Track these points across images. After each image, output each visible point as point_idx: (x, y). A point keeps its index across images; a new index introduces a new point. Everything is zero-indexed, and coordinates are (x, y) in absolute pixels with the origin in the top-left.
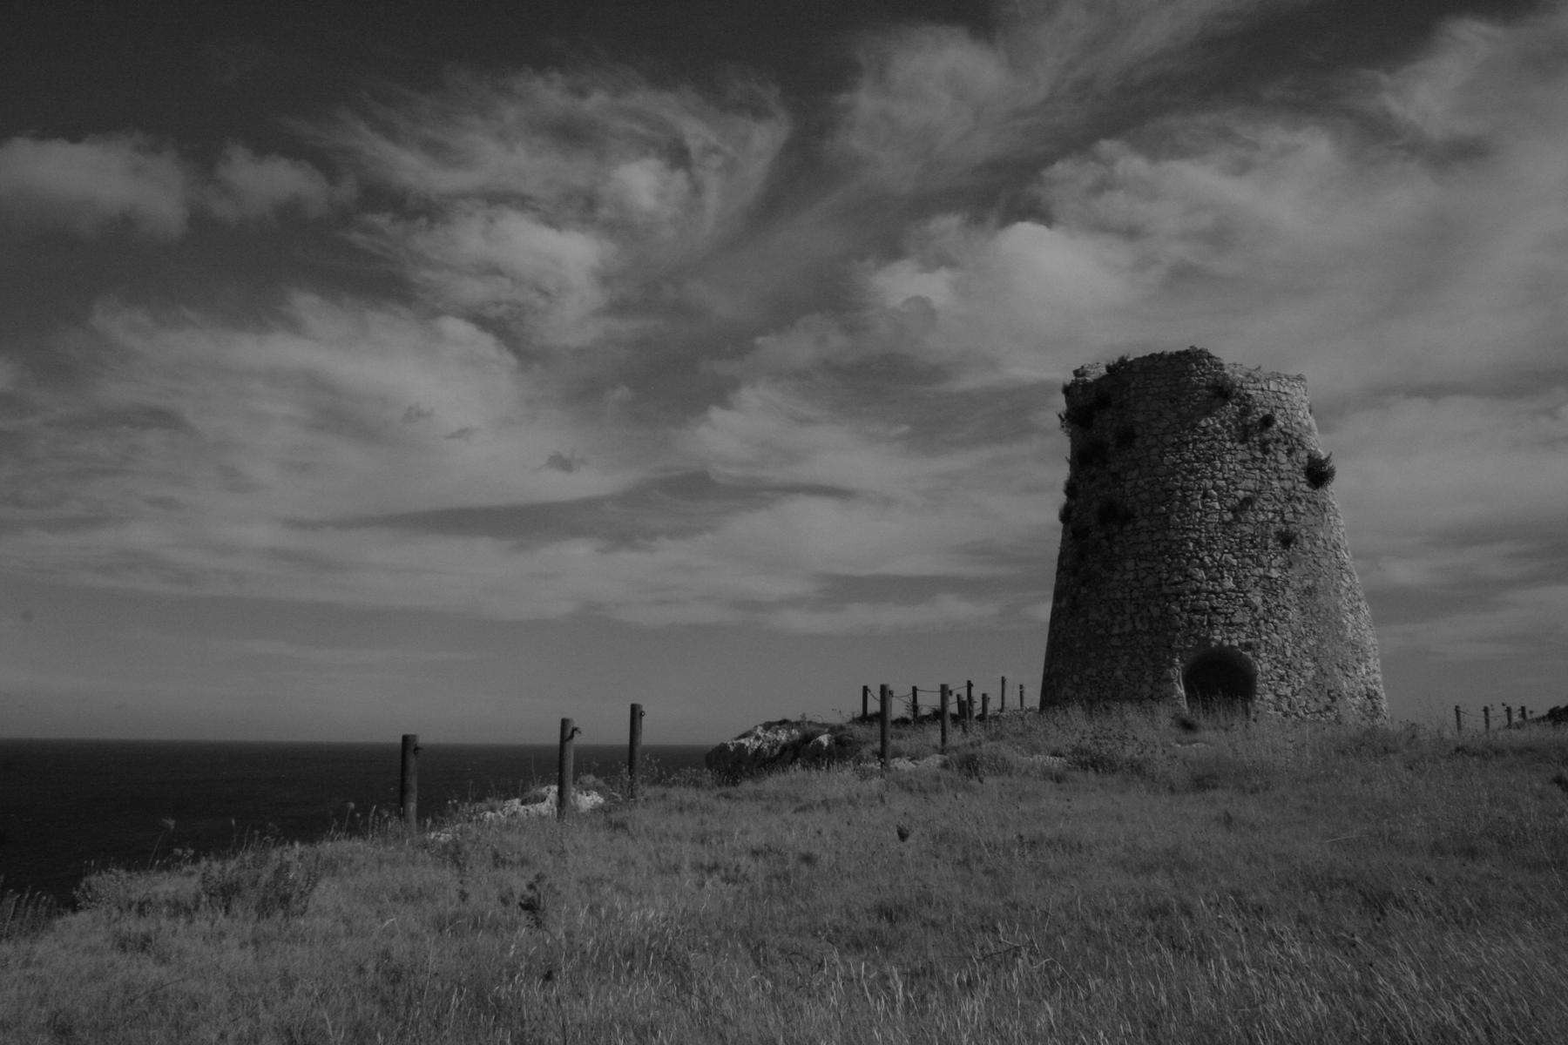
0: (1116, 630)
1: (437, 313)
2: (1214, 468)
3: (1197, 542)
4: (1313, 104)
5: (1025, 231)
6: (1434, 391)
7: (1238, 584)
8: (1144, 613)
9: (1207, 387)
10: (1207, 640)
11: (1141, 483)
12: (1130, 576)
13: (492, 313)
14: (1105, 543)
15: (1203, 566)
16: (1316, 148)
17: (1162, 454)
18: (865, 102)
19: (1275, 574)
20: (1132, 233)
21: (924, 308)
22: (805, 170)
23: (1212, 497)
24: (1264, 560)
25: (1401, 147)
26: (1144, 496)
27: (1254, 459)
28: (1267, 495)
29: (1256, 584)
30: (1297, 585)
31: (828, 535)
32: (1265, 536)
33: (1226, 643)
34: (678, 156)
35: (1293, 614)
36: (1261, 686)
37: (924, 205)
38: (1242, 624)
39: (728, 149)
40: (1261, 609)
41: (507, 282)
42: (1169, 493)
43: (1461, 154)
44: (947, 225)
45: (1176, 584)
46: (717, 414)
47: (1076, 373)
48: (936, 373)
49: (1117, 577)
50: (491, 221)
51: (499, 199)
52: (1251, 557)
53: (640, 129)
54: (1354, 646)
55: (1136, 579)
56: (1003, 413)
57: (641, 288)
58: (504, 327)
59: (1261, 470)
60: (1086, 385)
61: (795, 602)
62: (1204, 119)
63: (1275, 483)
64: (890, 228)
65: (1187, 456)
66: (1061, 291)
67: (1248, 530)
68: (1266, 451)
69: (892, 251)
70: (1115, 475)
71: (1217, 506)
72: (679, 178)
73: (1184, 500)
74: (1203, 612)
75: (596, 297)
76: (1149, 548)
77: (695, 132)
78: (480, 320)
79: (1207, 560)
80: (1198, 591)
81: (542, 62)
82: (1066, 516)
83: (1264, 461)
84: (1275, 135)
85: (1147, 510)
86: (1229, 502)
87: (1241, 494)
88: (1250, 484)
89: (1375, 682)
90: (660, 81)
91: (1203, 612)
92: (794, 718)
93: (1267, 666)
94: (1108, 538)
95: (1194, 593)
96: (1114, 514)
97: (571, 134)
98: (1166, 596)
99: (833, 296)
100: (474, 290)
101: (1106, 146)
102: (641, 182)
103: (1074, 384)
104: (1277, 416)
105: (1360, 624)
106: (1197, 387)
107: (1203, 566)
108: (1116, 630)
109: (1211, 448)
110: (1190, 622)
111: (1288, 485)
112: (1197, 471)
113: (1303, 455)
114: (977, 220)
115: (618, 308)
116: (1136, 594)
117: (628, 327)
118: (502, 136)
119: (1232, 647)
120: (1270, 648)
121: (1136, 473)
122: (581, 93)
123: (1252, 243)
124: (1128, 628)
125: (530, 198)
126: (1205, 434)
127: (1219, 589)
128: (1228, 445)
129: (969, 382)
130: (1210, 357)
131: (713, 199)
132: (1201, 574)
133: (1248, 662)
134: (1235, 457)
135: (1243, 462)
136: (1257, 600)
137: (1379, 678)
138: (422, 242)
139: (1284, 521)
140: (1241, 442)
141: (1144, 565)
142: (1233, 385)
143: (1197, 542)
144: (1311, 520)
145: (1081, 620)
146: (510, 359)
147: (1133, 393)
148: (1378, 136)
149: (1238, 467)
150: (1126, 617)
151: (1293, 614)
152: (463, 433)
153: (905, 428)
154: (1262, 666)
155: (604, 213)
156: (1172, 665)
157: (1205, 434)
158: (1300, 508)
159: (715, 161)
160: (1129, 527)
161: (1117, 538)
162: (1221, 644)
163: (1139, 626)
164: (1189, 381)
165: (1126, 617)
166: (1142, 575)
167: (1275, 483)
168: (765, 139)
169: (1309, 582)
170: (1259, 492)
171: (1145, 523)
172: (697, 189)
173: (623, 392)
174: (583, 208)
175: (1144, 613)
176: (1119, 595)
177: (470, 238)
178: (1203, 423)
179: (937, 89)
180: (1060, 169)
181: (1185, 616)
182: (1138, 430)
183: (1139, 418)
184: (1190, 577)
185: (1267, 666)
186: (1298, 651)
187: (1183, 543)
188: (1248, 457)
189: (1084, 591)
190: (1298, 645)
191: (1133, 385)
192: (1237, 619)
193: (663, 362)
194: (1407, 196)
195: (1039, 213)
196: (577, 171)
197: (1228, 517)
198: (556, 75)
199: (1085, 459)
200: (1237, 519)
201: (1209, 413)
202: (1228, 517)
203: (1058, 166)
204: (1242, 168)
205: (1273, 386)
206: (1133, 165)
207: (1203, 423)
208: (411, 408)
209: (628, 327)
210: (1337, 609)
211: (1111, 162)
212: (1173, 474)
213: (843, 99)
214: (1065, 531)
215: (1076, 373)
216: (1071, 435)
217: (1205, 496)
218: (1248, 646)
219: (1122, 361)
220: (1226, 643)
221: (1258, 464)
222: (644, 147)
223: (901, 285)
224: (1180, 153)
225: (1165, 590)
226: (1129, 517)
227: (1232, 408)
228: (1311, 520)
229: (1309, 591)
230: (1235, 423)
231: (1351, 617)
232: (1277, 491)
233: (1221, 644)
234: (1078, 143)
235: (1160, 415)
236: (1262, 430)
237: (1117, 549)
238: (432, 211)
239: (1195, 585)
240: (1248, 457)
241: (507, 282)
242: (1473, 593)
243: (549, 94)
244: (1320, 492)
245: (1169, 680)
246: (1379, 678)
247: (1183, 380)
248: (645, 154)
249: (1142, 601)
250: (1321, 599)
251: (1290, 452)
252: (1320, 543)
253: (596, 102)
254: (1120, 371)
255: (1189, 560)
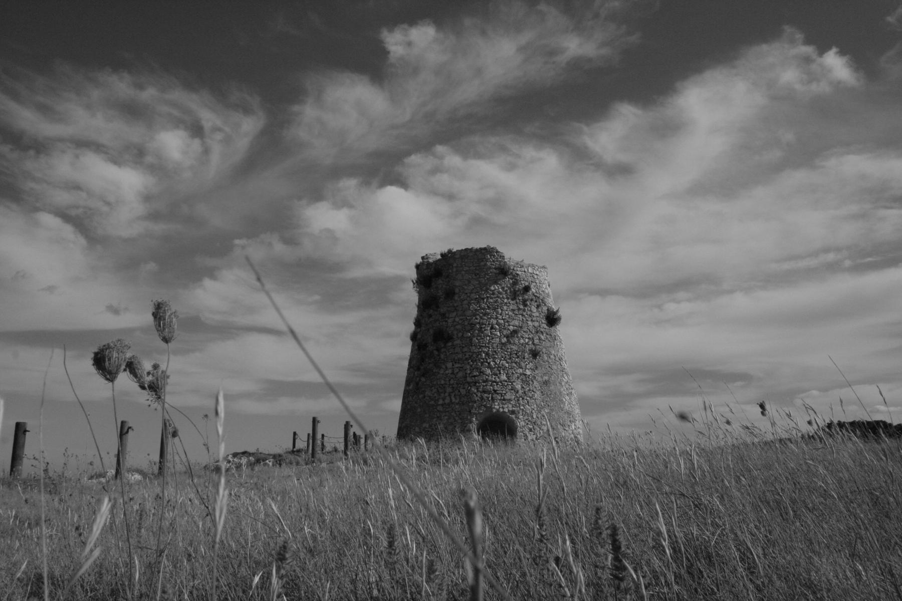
0: (441, 402)
1: (37, 210)
2: (497, 313)
3: (487, 354)
4: (549, 137)
5: (392, 193)
6: (603, 293)
7: (508, 377)
8: (457, 392)
9: (495, 269)
10: (491, 408)
11: (457, 319)
12: (450, 371)
13: (73, 212)
14: (436, 352)
15: (489, 367)
16: (550, 160)
17: (469, 304)
18: (309, 111)
19: (528, 372)
20: (450, 197)
21: (331, 235)
22: (271, 146)
23: (495, 329)
24: (523, 365)
25: (592, 164)
26: (459, 327)
27: (519, 309)
28: (525, 329)
29: (518, 378)
30: (540, 379)
31: (273, 357)
32: (524, 351)
33: (501, 410)
34: (197, 130)
35: (538, 395)
36: (519, 434)
37: (337, 172)
38: (510, 400)
39: (227, 129)
40: (520, 392)
41: (84, 195)
42: (472, 325)
43: (620, 171)
44: (349, 184)
45: (475, 376)
46: (208, 283)
47: (423, 258)
48: (337, 267)
49: (442, 372)
50: (77, 157)
51: (83, 144)
52: (516, 363)
53: (175, 112)
54: (568, 413)
55: (453, 373)
56: (377, 292)
57: (168, 205)
58: (80, 221)
59: (523, 315)
60: (429, 264)
61: (248, 395)
62: (493, 140)
63: (530, 323)
64: (317, 183)
65: (483, 305)
66: (412, 223)
67: (515, 348)
68: (525, 305)
69: (317, 196)
70: (443, 315)
71: (498, 334)
72: (196, 144)
73: (480, 330)
74: (489, 392)
75: (140, 209)
76: (460, 356)
77: (208, 118)
78: (64, 215)
79: (492, 363)
80: (486, 381)
81: (118, 65)
82: (414, 337)
83: (524, 310)
84: (529, 152)
85: (460, 335)
86: (505, 332)
87: (511, 328)
88: (517, 323)
89: (579, 433)
90: (189, 86)
91: (489, 392)
92: (252, 450)
93: (523, 423)
94: (438, 350)
95: (484, 382)
96: (442, 337)
97: (133, 111)
98: (469, 383)
99: (280, 222)
100: (62, 198)
101: (440, 149)
102: (173, 143)
103: (422, 264)
104: (532, 286)
105: (571, 404)
106: (490, 268)
107: (489, 367)
108: (441, 402)
109: (496, 302)
110: (482, 398)
111: (536, 324)
112: (488, 314)
113: (545, 309)
114: (366, 183)
115: (154, 216)
116: (452, 382)
117: (159, 228)
118: (88, 107)
119: (504, 412)
120: (525, 413)
121: (455, 314)
122: (140, 87)
123: (519, 199)
124: (447, 401)
125: (104, 146)
126: (493, 294)
127: (498, 380)
128: (506, 301)
129: (357, 273)
130: (497, 252)
131: (215, 158)
132: (489, 371)
133: (513, 422)
134: (509, 307)
135: (513, 310)
136: (519, 387)
137: (581, 432)
138: (30, 164)
139: (533, 344)
140: (512, 300)
141: (457, 365)
142: (509, 268)
143: (487, 354)
144: (548, 344)
145: (421, 396)
146: (82, 241)
147: (455, 270)
148: (580, 158)
149: (511, 313)
150: (447, 394)
151: (538, 395)
152: (51, 289)
153: (317, 297)
154: (520, 423)
155: (149, 159)
156: (471, 422)
157: (493, 294)
158: (542, 337)
159: (219, 136)
160: (450, 344)
161: (443, 350)
162: (498, 410)
163: (454, 400)
164: (486, 265)
165: (447, 394)
166: (456, 371)
167: (530, 323)
168: (250, 126)
169: (546, 378)
170: (521, 327)
171: (458, 342)
172: (206, 151)
173: (152, 266)
174: (136, 155)
175: (457, 392)
176: (443, 382)
177: (62, 166)
178: (492, 288)
179: (348, 107)
180: (415, 159)
181: (479, 394)
182: (457, 290)
183: (457, 283)
184: (482, 373)
185: (523, 423)
186: (539, 416)
187: (479, 353)
188: (515, 307)
189: (423, 379)
190: (540, 412)
191: (455, 265)
192: (507, 397)
193: (180, 247)
194: (594, 190)
195: (401, 182)
196: (134, 133)
197: (504, 340)
198: (126, 76)
199: (426, 305)
200: (509, 342)
201: (496, 283)
202: (504, 340)
203: (413, 157)
204: (511, 167)
205: (530, 270)
206: (453, 160)
207: (492, 288)
208: (18, 272)
209: (159, 228)
210: (561, 393)
211: (441, 158)
212: (475, 315)
213: (296, 108)
214: (413, 346)
215: (423, 258)
216: (419, 292)
217: (492, 328)
218: (513, 412)
219: (450, 251)
220: (501, 410)
221: (521, 312)
222: (177, 123)
223: (324, 218)
224: (479, 156)
225: (469, 379)
226: (450, 338)
227: (508, 281)
228: (548, 344)
229: (546, 383)
230: (510, 288)
231: (567, 398)
232: (530, 327)
233: (498, 410)
234: (425, 146)
235: (469, 282)
236: (523, 294)
237: (442, 356)
238: (40, 147)
239: (485, 377)
240: (515, 307)
241: (84, 195)
242: (619, 401)
243: (121, 86)
244: (553, 329)
245: (469, 430)
246: (581, 432)
247: (482, 263)
248: (177, 127)
249: (455, 386)
250: (552, 387)
251: (538, 307)
252: (552, 357)
253: (149, 94)
254: (448, 257)
255: (482, 363)
